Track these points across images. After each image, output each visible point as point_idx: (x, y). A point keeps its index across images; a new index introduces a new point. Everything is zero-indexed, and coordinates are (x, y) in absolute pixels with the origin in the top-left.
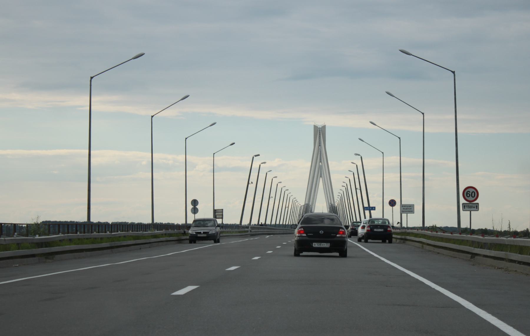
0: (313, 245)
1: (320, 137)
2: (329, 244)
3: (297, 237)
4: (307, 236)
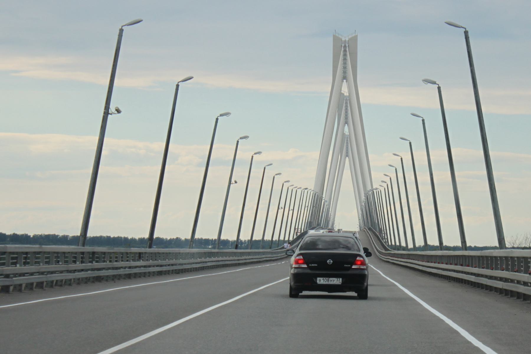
0: (318, 282)
1: (345, 59)
2: (341, 279)
3: (293, 269)
4: (309, 267)
